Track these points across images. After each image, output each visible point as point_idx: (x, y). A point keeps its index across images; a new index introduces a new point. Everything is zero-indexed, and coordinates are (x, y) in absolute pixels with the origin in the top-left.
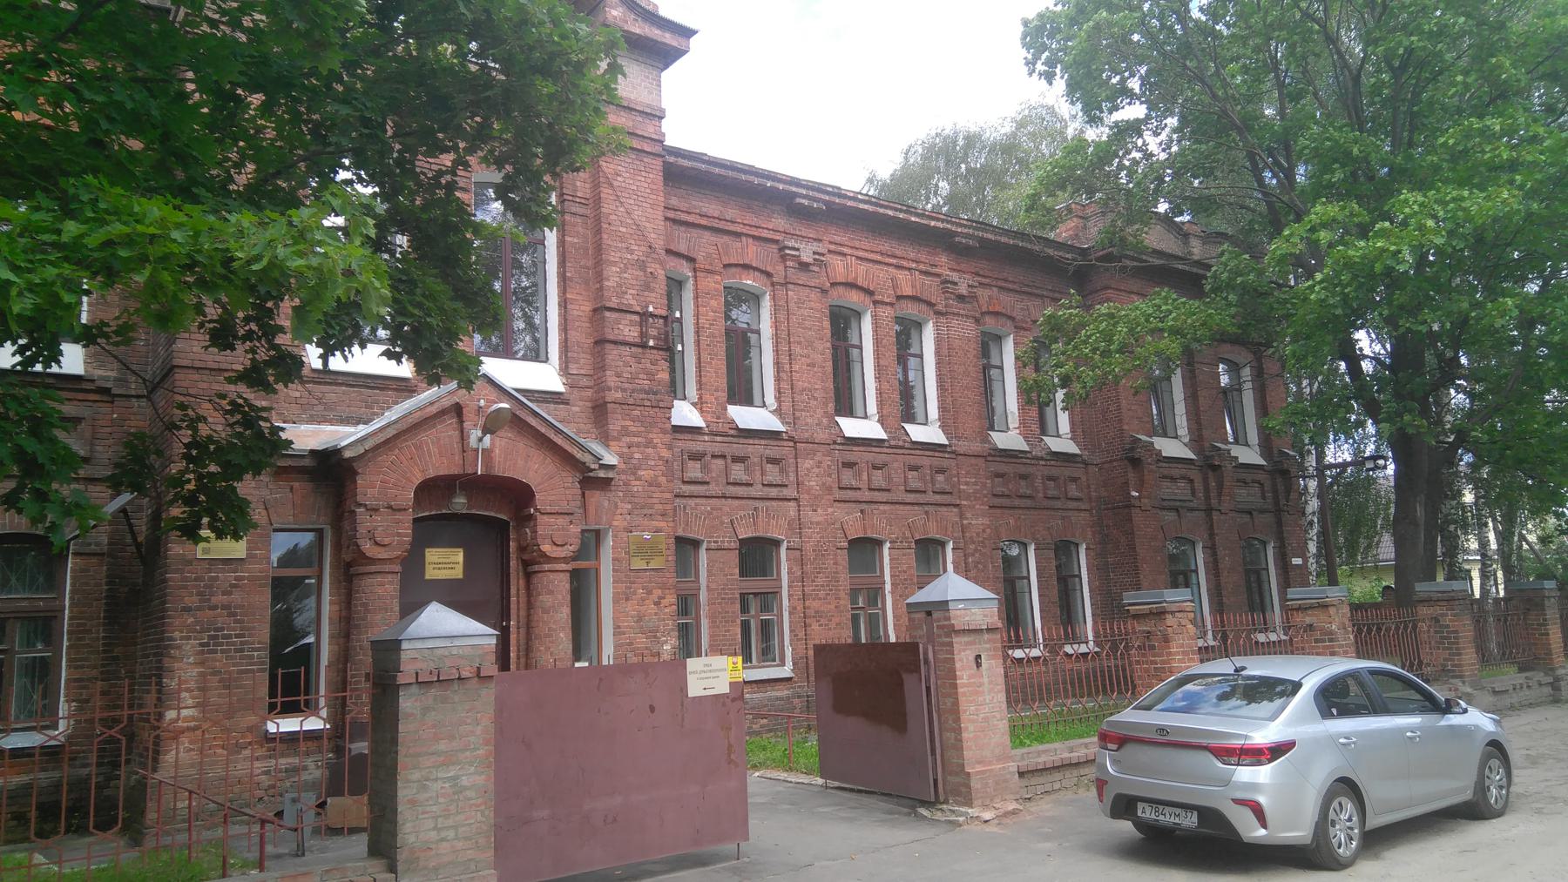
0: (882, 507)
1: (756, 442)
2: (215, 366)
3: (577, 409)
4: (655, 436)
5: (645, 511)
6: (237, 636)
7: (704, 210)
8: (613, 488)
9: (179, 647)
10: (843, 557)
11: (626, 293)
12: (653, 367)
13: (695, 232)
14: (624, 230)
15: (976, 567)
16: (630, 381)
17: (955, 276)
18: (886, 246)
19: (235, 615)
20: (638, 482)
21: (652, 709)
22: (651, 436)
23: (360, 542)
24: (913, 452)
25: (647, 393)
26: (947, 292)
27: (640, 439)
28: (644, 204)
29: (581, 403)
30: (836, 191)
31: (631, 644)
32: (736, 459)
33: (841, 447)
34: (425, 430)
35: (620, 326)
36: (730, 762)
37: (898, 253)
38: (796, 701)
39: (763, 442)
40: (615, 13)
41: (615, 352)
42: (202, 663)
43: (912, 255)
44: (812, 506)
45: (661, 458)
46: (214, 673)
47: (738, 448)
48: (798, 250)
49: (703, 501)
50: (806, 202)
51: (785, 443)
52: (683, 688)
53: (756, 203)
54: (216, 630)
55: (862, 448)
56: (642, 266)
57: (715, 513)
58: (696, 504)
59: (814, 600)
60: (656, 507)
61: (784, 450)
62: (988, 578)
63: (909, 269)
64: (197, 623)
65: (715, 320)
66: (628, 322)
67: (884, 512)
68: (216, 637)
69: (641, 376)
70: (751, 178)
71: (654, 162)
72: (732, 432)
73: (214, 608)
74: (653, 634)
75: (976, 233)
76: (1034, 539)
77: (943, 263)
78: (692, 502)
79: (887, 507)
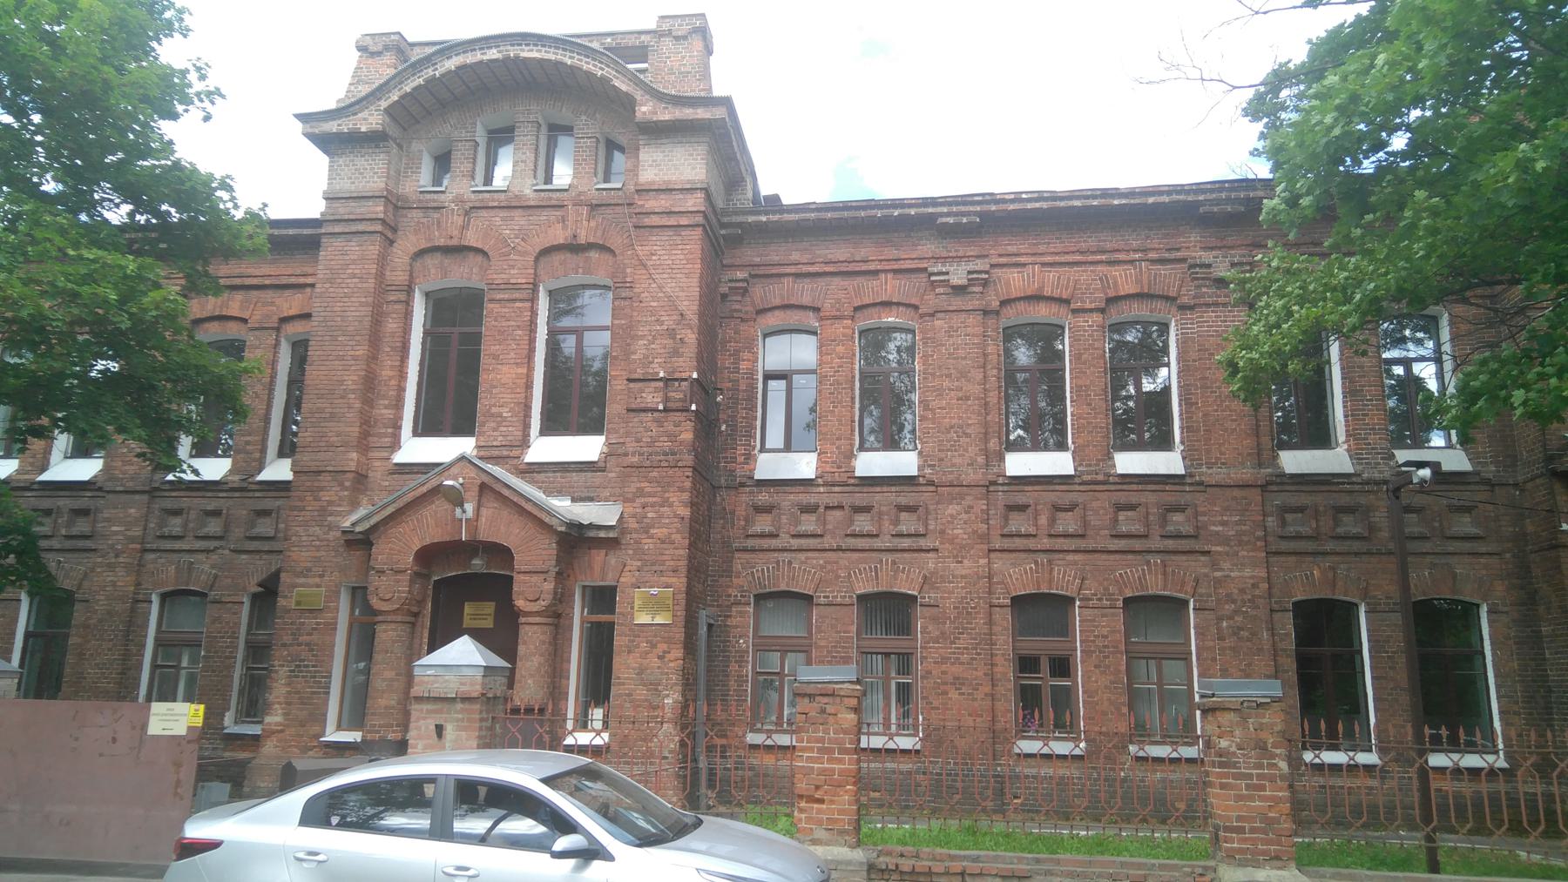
0: (1070, 557)
1: (885, 489)
2: (315, 469)
3: (613, 475)
4: (672, 494)
5: (655, 568)
6: (313, 666)
7: (830, 256)
8: (623, 547)
9: (276, 672)
10: (1004, 618)
11: (653, 362)
12: (675, 429)
13: (822, 282)
14: (655, 304)
15: (1235, 634)
16: (651, 444)
17: (1207, 257)
18: (1091, 242)
19: (313, 650)
20: (650, 541)
21: (114, 740)
22: (667, 495)
23: (369, 597)
24: (1125, 487)
25: (666, 454)
26: (1197, 279)
27: (654, 499)
28: (678, 276)
29: (618, 469)
30: (988, 198)
31: (630, 695)
32: (858, 510)
33: (1006, 488)
34: (426, 507)
35: (644, 395)
36: (176, 794)
37: (1108, 246)
38: (920, 777)
39: (893, 489)
40: (644, 109)
41: (636, 420)
42: (288, 685)
43: (1135, 244)
44: (955, 557)
45: (676, 516)
46: (296, 693)
47: (860, 499)
48: (947, 273)
49: (816, 554)
50: (951, 220)
51: (924, 489)
52: (144, 726)
53: (896, 235)
54: (301, 661)
55: (1036, 488)
56: (671, 333)
57: (829, 567)
58: (807, 558)
59: (953, 664)
60: (667, 563)
61: (925, 497)
62: (1262, 649)
63: (1132, 262)
64: (289, 655)
65: (841, 366)
66: (651, 390)
67: (1075, 563)
68: (299, 666)
69: (661, 439)
70: (873, 212)
71: (693, 233)
72: (852, 481)
73: (300, 645)
74: (654, 687)
75: (1233, 195)
76: (1365, 596)
77: (1193, 246)
78: (802, 556)
79: (1078, 557)
